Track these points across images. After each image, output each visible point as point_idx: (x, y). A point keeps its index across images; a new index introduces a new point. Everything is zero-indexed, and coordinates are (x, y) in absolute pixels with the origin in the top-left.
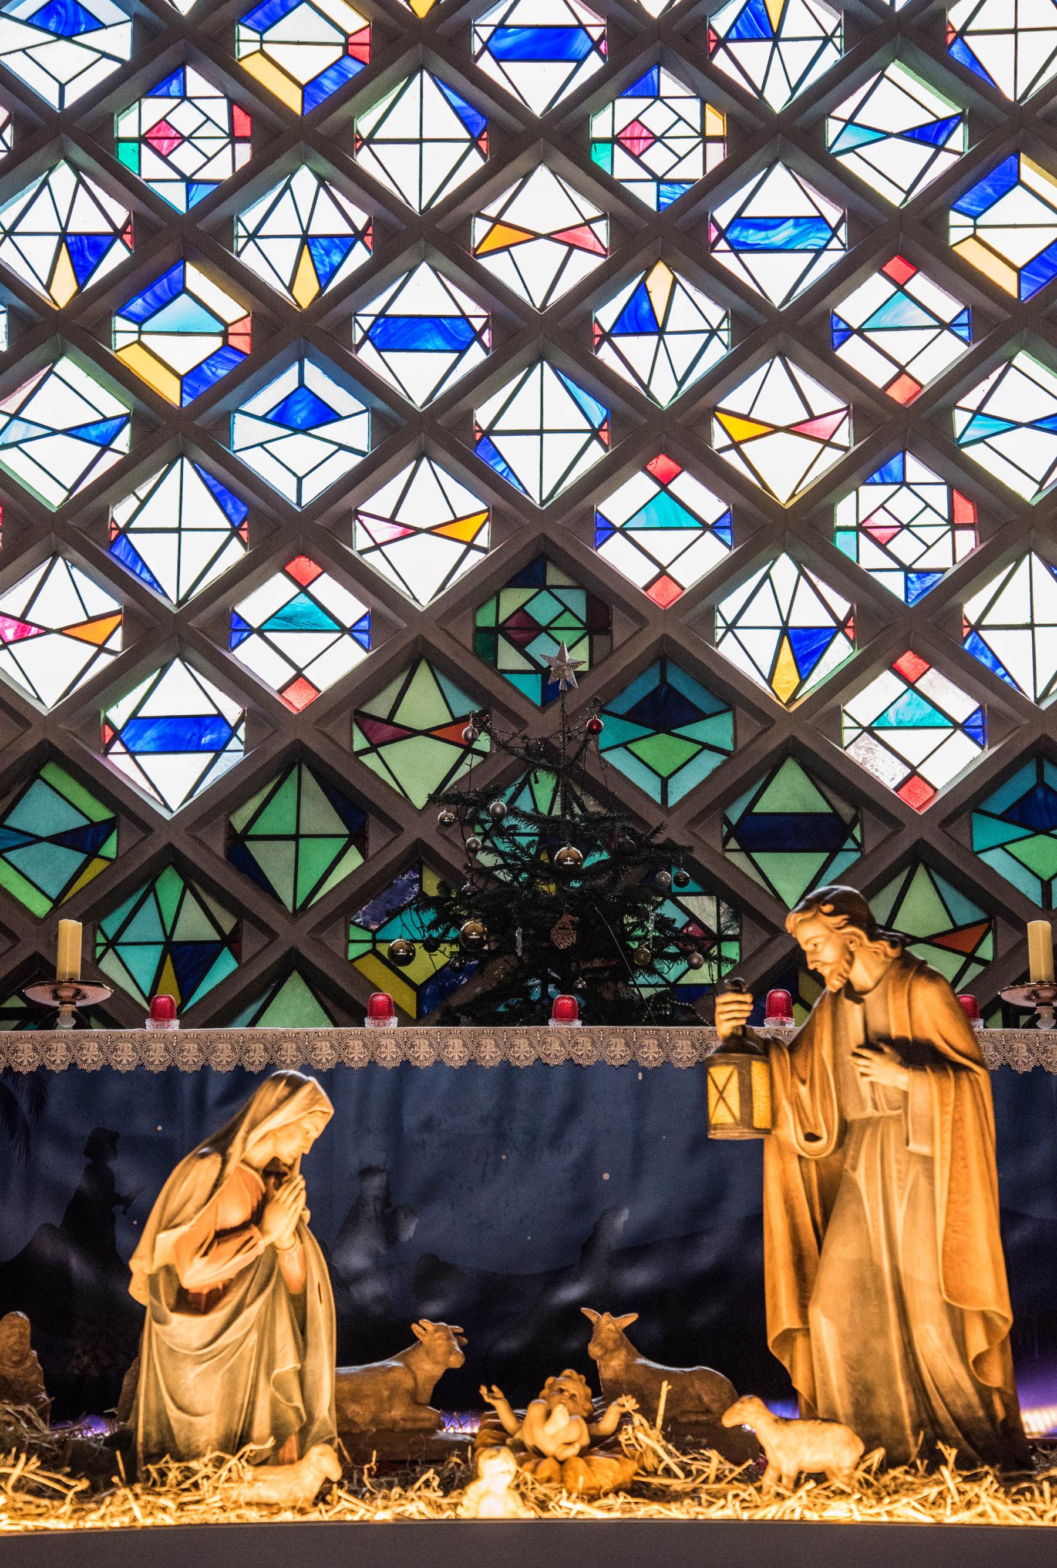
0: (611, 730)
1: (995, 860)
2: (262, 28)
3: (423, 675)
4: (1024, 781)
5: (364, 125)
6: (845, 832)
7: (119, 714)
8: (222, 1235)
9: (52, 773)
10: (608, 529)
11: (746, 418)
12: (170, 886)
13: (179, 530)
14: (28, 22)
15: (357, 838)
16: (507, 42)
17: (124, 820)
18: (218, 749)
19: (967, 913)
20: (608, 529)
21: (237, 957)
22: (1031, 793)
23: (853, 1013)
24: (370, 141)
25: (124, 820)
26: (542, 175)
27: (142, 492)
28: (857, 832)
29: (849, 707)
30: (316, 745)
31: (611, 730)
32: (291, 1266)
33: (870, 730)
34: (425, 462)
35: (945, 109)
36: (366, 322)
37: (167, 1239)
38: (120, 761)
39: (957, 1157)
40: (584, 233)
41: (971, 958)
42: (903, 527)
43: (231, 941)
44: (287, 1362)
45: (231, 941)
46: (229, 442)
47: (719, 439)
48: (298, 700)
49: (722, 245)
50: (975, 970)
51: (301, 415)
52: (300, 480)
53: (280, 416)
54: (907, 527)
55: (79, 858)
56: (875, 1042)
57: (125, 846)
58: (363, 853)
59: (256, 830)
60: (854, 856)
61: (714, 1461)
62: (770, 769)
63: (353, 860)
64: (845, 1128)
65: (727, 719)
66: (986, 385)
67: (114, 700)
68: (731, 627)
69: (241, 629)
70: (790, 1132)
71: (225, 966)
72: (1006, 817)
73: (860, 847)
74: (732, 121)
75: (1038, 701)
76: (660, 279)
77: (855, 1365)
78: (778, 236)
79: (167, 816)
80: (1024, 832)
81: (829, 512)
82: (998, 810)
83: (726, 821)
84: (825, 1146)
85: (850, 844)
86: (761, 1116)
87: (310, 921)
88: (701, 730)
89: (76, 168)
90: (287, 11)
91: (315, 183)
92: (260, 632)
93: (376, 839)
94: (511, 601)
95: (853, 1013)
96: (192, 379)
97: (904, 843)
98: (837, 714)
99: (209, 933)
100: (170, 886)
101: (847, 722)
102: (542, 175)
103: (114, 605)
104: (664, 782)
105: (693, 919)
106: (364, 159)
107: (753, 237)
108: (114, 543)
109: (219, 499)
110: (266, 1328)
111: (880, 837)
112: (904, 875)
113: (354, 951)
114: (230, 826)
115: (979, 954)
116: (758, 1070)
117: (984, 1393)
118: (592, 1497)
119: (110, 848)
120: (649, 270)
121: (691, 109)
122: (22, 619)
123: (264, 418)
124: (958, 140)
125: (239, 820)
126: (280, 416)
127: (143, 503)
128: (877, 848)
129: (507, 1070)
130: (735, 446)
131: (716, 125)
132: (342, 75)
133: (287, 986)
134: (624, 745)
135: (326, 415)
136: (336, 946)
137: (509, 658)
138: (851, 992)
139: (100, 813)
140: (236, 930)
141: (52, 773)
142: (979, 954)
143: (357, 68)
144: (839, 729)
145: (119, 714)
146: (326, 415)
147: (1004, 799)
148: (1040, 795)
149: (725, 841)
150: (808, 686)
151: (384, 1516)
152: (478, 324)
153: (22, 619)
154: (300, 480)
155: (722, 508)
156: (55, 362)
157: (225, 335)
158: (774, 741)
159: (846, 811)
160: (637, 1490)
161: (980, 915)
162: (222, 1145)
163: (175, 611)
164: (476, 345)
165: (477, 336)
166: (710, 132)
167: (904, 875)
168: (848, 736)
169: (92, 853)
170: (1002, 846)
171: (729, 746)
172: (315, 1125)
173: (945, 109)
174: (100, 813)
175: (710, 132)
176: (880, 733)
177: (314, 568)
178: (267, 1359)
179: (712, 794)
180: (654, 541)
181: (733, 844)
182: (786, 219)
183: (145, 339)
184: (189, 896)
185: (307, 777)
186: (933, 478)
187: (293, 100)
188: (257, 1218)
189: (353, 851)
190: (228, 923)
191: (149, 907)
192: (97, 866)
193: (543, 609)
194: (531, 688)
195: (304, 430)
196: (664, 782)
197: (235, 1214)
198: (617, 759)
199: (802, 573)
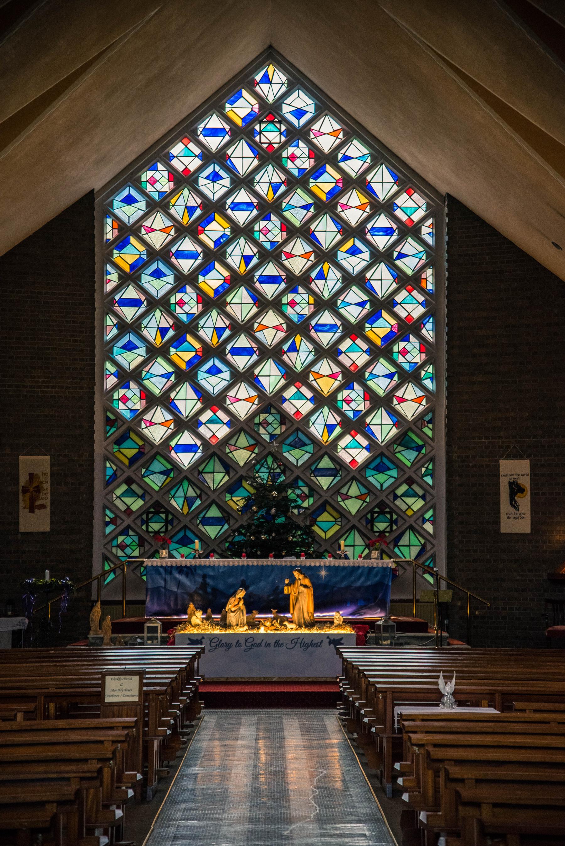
0: (285, 448)
1: (371, 479)
2: (204, 275)
3: (242, 433)
4: (378, 461)
5: (228, 300)
6: (338, 472)
7: (173, 443)
8: (235, 605)
9: (158, 457)
10: (285, 400)
11: (317, 373)
12: (185, 484)
13: (186, 399)
14: (149, 275)
15: (228, 473)
16: (261, 279)
17: (175, 469)
18: (196, 452)
19: (364, 491)
20: (285, 400)
21: (201, 500)
22: (379, 464)
23: (299, 582)
24: (230, 303)
25: (175, 469)
26: (271, 312)
27: (177, 390)
28: (340, 473)
29: (339, 443)
30: (218, 452)
31: (285, 448)
32: (242, 608)
33: (344, 449)
34: (243, 383)
35: (365, 298)
36: (229, 349)
37: (230, 606)
38: (173, 454)
39: (309, 597)
40: (280, 327)
41: (364, 501)
42: (353, 400)
43: (199, 496)
44: (242, 617)
45: (199, 496)
46: (197, 379)
47: (311, 378)
48: (214, 441)
49: (313, 330)
50: (365, 504)
51: (214, 371)
52: (214, 387)
53: (209, 371)
54: (354, 400)
55: (164, 477)
56: (301, 585)
57: (175, 475)
58: (229, 476)
59: (205, 471)
60: (340, 478)
61: (283, 627)
62: (322, 457)
63: (227, 478)
64: (299, 593)
65: (312, 446)
66: (372, 367)
67: (172, 440)
68: (313, 424)
69: (200, 424)
70: (293, 593)
71: (198, 502)
72: (373, 469)
73: (341, 476)
74: (315, 300)
75: (382, 442)
76: (298, 338)
77: (298, 617)
78: (326, 329)
79: (185, 469)
80: (377, 473)
81: (336, 397)
82: (372, 468)
83: (311, 469)
84: (296, 594)
85: (339, 475)
86: (290, 592)
87: (217, 493)
88: (306, 448)
89: (161, 311)
90: (210, 271)
91: (217, 314)
92: (205, 424)
93: (232, 474)
94: (263, 416)
95: (299, 582)
96: (189, 363)
97: (351, 476)
98: (337, 445)
99: (194, 495)
100: (185, 484)
101: (339, 447)
102: (271, 312)
103: (171, 418)
104: (297, 460)
105: (303, 492)
106: (228, 308)
107: (320, 328)
108: (171, 403)
109: (196, 393)
110: (240, 614)
111: (345, 474)
112: (350, 483)
113: (227, 499)
114: (199, 470)
115: (366, 500)
116: (289, 587)
117: (311, 620)
118: (271, 630)
119: (172, 475)
120: (296, 336)
121: (306, 296)
122: (151, 421)
123: (205, 372)
124: (368, 306)
125: (201, 468)
126: (209, 371)
127: (178, 393)
128: (345, 476)
129: (262, 566)
130: (315, 380)
131: (312, 301)
132: (223, 287)
133: (211, 508)
134: (288, 452)
135: (219, 371)
136: (223, 498)
137: (262, 431)
138: (300, 579)
139: (169, 467)
140: (201, 494)
141: (158, 457)
142: (366, 500)
143: (227, 285)
144: (337, 448)
145: (173, 443)
146: (219, 371)
147: (373, 465)
148: (381, 464)
149: (311, 474)
150: (330, 438)
151: (252, 632)
152: (255, 349)
153: (151, 421)
154: (214, 387)
155: (312, 395)
156: (157, 358)
157: (196, 351)
158: (322, 452)
159: (338, 467)
160: (276, 630)
161: (367, 492)
162: (235, 596)
163: (184, 419)
164: (255, 354)
165: (255, 352)
166: (310, 303)
167: (350, 483)
168: (339, 450)
169: (168, 476)
170: (372, 476)
171: (312, 452)
172: (244, 594)
173: (365, 298)
174: (169, 467)
175: (310, 303)
176: (346, 449)
177: (217, 408)
178: (240, 617)
179: (308, 464)
180: (296, 403)
181: (312, 475)
182: (328, 324)
183: (177, 353)
184: (190, 486)
185: (216, 458)
186: (361, 388)
187: (211, 294)
188: (238, 604)
189: (227, 476)
190: (199, 492)
191: (181, 489)
192: (169, 479)
193: (270, 419)
194: (267, 438)
195: (214, 375)
196: (297, 460)
197: (236, 603)
198: (286, 454)
199: (330, 411)
